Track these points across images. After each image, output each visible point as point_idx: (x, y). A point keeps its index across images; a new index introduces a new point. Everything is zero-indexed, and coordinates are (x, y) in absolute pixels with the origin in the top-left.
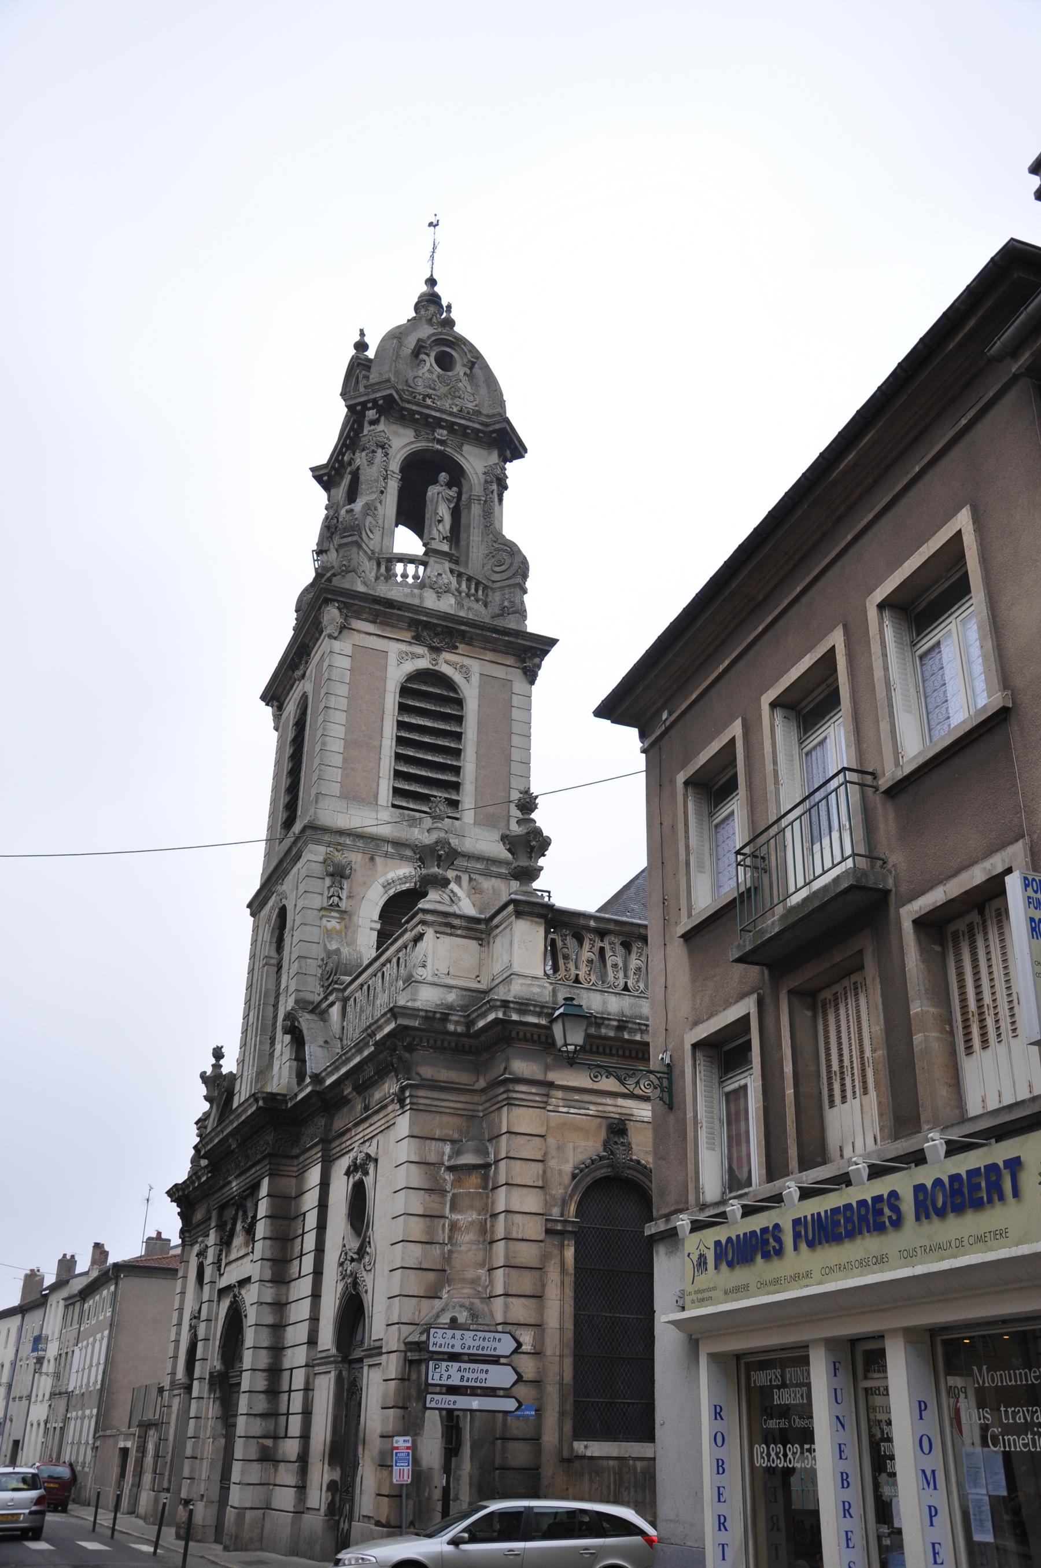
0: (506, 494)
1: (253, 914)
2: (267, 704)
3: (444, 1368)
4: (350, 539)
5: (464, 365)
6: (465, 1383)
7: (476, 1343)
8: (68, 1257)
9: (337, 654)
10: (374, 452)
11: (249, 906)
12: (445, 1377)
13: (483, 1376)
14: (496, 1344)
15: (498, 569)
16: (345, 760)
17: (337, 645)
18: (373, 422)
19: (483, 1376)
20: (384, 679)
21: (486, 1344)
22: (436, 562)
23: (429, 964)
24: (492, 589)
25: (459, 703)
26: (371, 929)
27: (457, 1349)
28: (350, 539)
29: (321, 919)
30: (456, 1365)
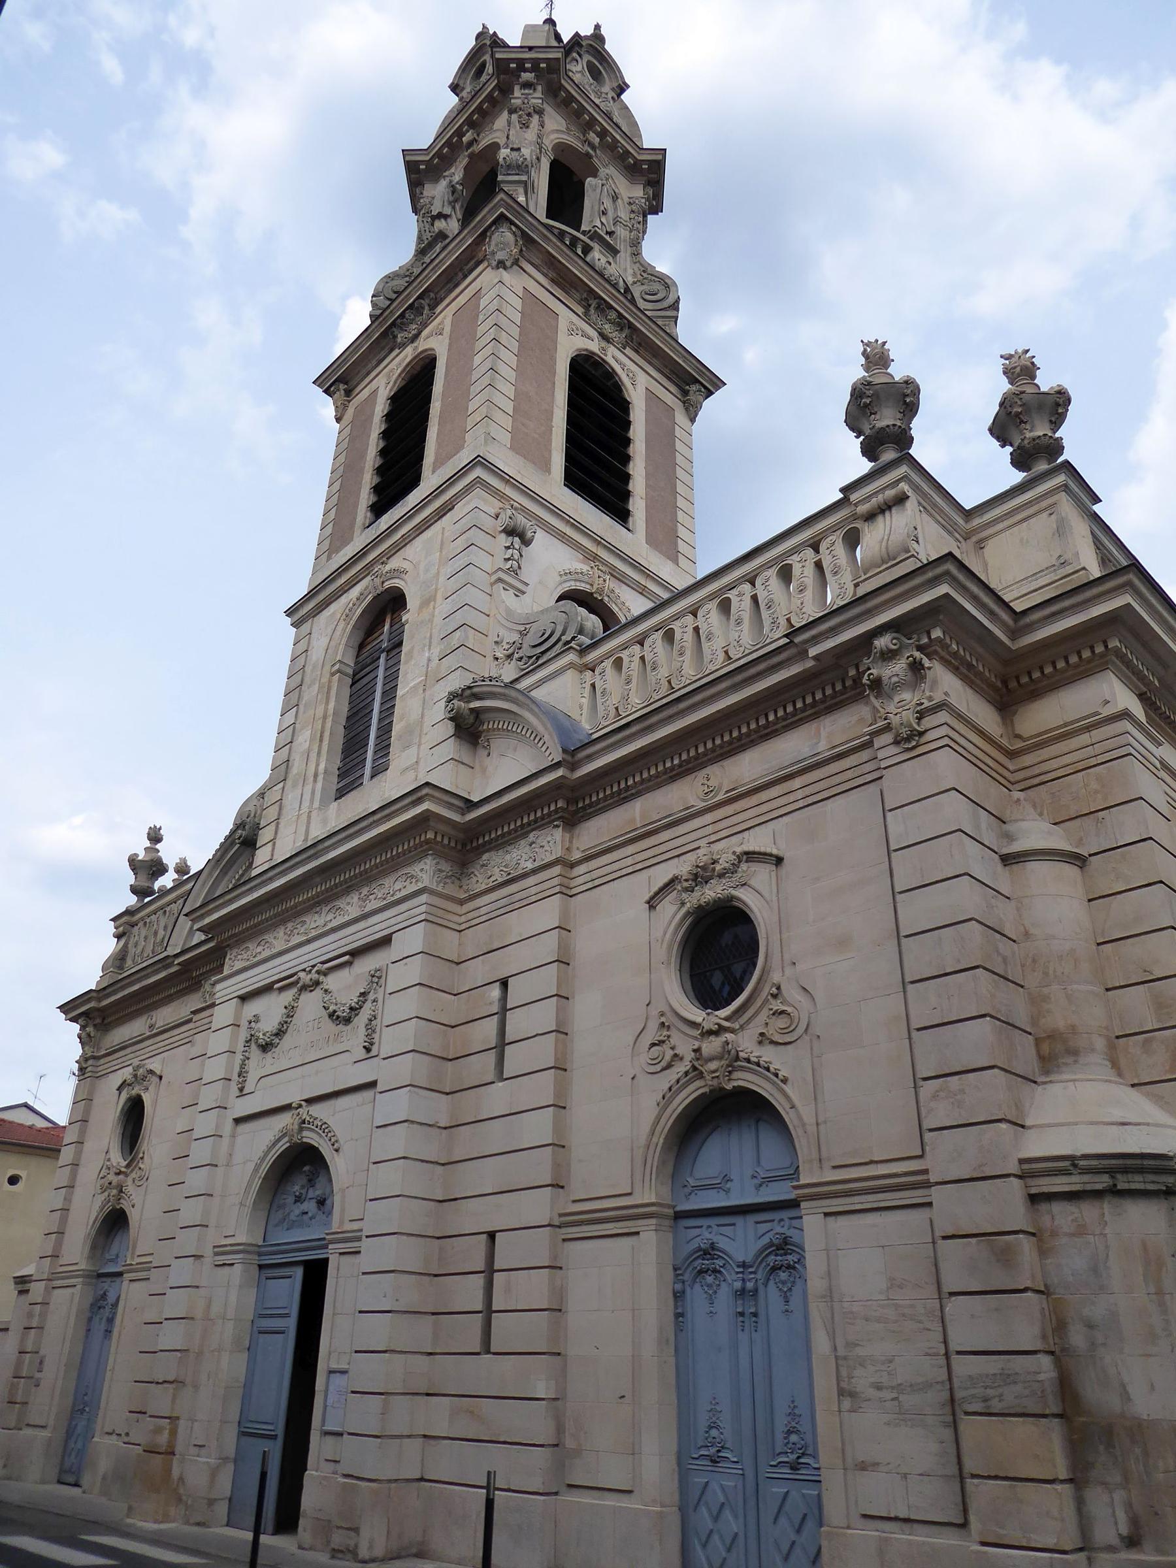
5: (613, 89)
10: (529, 115)
11: (289, 613)
18: (527, 85)
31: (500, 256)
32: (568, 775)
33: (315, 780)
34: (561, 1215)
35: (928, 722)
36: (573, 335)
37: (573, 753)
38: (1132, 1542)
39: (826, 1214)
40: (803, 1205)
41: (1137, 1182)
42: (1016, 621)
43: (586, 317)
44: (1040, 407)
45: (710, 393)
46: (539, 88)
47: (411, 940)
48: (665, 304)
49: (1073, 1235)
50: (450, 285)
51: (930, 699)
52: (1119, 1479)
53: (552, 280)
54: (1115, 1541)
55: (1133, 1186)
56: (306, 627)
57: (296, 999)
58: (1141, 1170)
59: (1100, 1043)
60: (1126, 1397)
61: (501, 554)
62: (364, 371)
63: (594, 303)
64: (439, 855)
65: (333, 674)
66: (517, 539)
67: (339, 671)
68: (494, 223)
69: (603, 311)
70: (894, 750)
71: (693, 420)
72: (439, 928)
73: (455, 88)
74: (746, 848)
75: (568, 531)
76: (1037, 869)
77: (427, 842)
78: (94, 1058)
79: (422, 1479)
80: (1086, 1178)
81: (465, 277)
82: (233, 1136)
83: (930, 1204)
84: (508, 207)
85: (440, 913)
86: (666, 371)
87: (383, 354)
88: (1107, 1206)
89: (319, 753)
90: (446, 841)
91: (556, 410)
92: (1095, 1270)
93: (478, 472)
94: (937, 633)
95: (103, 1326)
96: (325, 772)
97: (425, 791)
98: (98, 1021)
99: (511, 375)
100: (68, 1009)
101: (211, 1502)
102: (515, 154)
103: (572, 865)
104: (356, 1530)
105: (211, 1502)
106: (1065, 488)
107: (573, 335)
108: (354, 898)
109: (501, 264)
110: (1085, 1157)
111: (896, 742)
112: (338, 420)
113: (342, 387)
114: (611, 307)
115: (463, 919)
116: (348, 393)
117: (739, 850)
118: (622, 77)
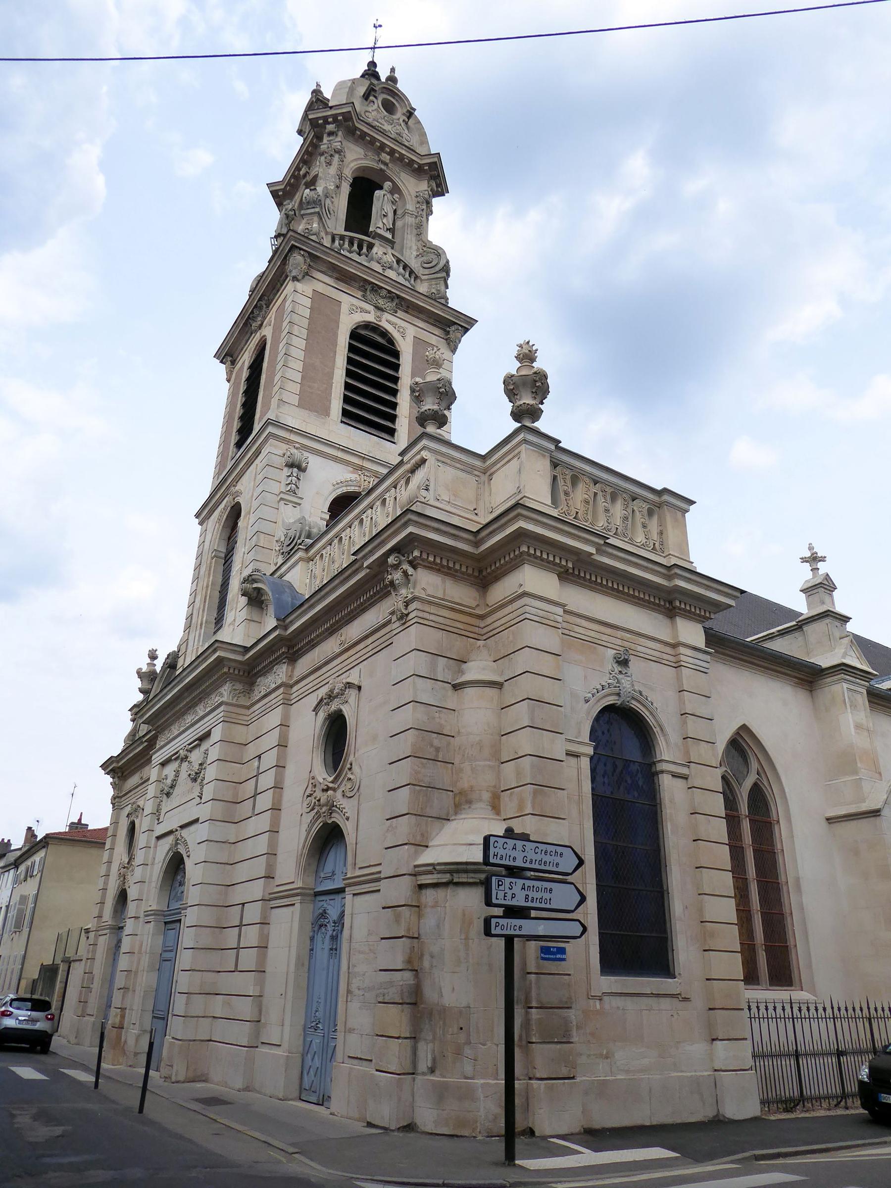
0: (430, 218)
1: (201, 523)
2: (221, 362)
3: (507, 885)
4: (312, 211)
5: (404, 114)
6: (529, 904)
7: (538, 857)
8: (6, 841)
9: (298, 296)
10: (331, 156)
11: (197, 516)
12: (509, 896)
13: (547, 896)
14: (557, 859)
15: (426, 265)
16: (303, 378)
17: (299, 286)
18: (330, 134)
19: (547, 896)
20: (337, 323)
21: (547, 858)
22: (381, 245)
23: (431, 488)
24: (422, 280)
25: (396, 354)
26: (322, 519)
27: (519, 863)
28: (312, 211)
29: (278, 502)
30: (520, 882)
31: (293, 274)
32: (283, 633)
33: (201, 628)
34: (270, 894)
35: (412, 607)
36: (353, 311)
37: (284, 620)
38: (432, 1070)
39: (354, 895)
40: (347, 889)
41: (463, 878)
42: (475, 537)
43: (365, 299)
44: (524, 384)
45: (466, 330)
46: (340, 133)
47: (216, 735)
48: (437, 269)
49: (433, 907)
50: (275, 291)
51: (412, 593)
52: (431, 1037)
53: (337, 279)
54: (425, 1070)
55: (461, 880)
56: (205, 524)
57: (180, 766)
58: (466, 871)
59: (486, 796)
60: (441, 995)
61: (284, 481)
62: (240, 348)
63: (369, 288)
64: (232, 680)
65: (212, 558)
66: (295, 470)
67: (215, 556)
68: (289, 251)
69: (376, 291)
70: (398, 624)
71: (454, 351)
72: (233, 725)
73: (300, 132)
74: (349, 680)
75: (340, 454)
76: (470, 691)
77: (225, 673)
78: (118, 797)
79: (211, 1040)
80: (439, 876)
81: (282, 285)
82: (156, 847)
83: (379, 891)
84: (296, 240)
85: (234, 715)
86: (431, 321)
87: (247, 337)
88: (450, 891)
89: (204, 610)
90: (236, 672)
91: (336, 371)
92: (438, 926)
93: (270, 429)
94: (416, 553)
95: (327, 945)
96: (206, 622)
97: (217, 645)
98: (120, 774)
99: (301, 355)
100: (104, 766)
101: (136, 1054)
102: (313, 192)
103: (291, 687)
104: (172, 1066)
105: (136, 1054)
106: (525, 441)
107: (353, 311)
108: (201, 706)
109: (295, 279)
110: (439, 864)
111: (398, 620)
112: (228, 381)
113: (229, 359)
114: (382, 288)
115: (249, 718)
116: (233, 363)
117: (344, 681)
118: (410, 104)
